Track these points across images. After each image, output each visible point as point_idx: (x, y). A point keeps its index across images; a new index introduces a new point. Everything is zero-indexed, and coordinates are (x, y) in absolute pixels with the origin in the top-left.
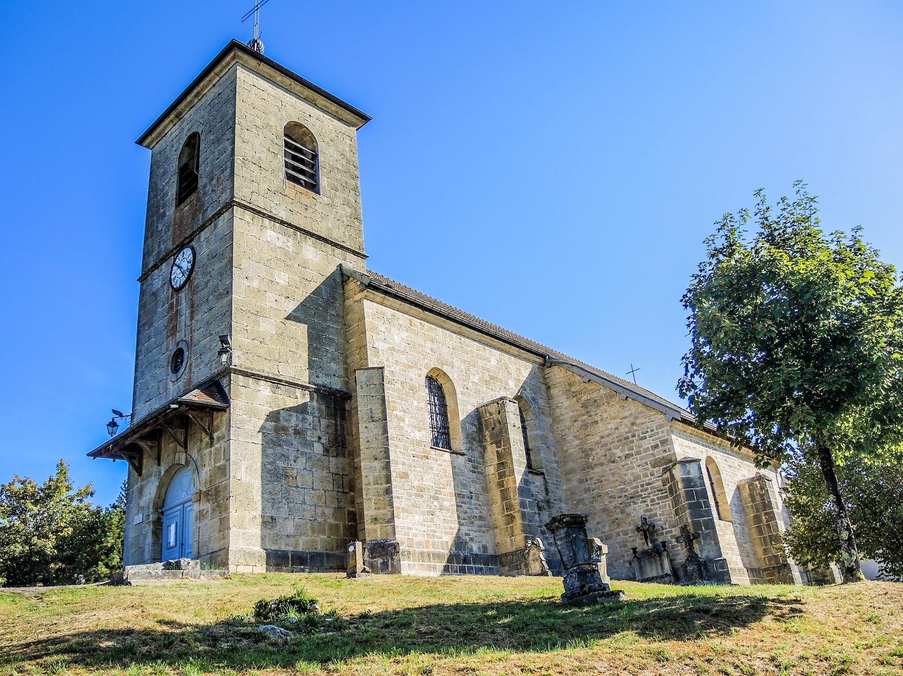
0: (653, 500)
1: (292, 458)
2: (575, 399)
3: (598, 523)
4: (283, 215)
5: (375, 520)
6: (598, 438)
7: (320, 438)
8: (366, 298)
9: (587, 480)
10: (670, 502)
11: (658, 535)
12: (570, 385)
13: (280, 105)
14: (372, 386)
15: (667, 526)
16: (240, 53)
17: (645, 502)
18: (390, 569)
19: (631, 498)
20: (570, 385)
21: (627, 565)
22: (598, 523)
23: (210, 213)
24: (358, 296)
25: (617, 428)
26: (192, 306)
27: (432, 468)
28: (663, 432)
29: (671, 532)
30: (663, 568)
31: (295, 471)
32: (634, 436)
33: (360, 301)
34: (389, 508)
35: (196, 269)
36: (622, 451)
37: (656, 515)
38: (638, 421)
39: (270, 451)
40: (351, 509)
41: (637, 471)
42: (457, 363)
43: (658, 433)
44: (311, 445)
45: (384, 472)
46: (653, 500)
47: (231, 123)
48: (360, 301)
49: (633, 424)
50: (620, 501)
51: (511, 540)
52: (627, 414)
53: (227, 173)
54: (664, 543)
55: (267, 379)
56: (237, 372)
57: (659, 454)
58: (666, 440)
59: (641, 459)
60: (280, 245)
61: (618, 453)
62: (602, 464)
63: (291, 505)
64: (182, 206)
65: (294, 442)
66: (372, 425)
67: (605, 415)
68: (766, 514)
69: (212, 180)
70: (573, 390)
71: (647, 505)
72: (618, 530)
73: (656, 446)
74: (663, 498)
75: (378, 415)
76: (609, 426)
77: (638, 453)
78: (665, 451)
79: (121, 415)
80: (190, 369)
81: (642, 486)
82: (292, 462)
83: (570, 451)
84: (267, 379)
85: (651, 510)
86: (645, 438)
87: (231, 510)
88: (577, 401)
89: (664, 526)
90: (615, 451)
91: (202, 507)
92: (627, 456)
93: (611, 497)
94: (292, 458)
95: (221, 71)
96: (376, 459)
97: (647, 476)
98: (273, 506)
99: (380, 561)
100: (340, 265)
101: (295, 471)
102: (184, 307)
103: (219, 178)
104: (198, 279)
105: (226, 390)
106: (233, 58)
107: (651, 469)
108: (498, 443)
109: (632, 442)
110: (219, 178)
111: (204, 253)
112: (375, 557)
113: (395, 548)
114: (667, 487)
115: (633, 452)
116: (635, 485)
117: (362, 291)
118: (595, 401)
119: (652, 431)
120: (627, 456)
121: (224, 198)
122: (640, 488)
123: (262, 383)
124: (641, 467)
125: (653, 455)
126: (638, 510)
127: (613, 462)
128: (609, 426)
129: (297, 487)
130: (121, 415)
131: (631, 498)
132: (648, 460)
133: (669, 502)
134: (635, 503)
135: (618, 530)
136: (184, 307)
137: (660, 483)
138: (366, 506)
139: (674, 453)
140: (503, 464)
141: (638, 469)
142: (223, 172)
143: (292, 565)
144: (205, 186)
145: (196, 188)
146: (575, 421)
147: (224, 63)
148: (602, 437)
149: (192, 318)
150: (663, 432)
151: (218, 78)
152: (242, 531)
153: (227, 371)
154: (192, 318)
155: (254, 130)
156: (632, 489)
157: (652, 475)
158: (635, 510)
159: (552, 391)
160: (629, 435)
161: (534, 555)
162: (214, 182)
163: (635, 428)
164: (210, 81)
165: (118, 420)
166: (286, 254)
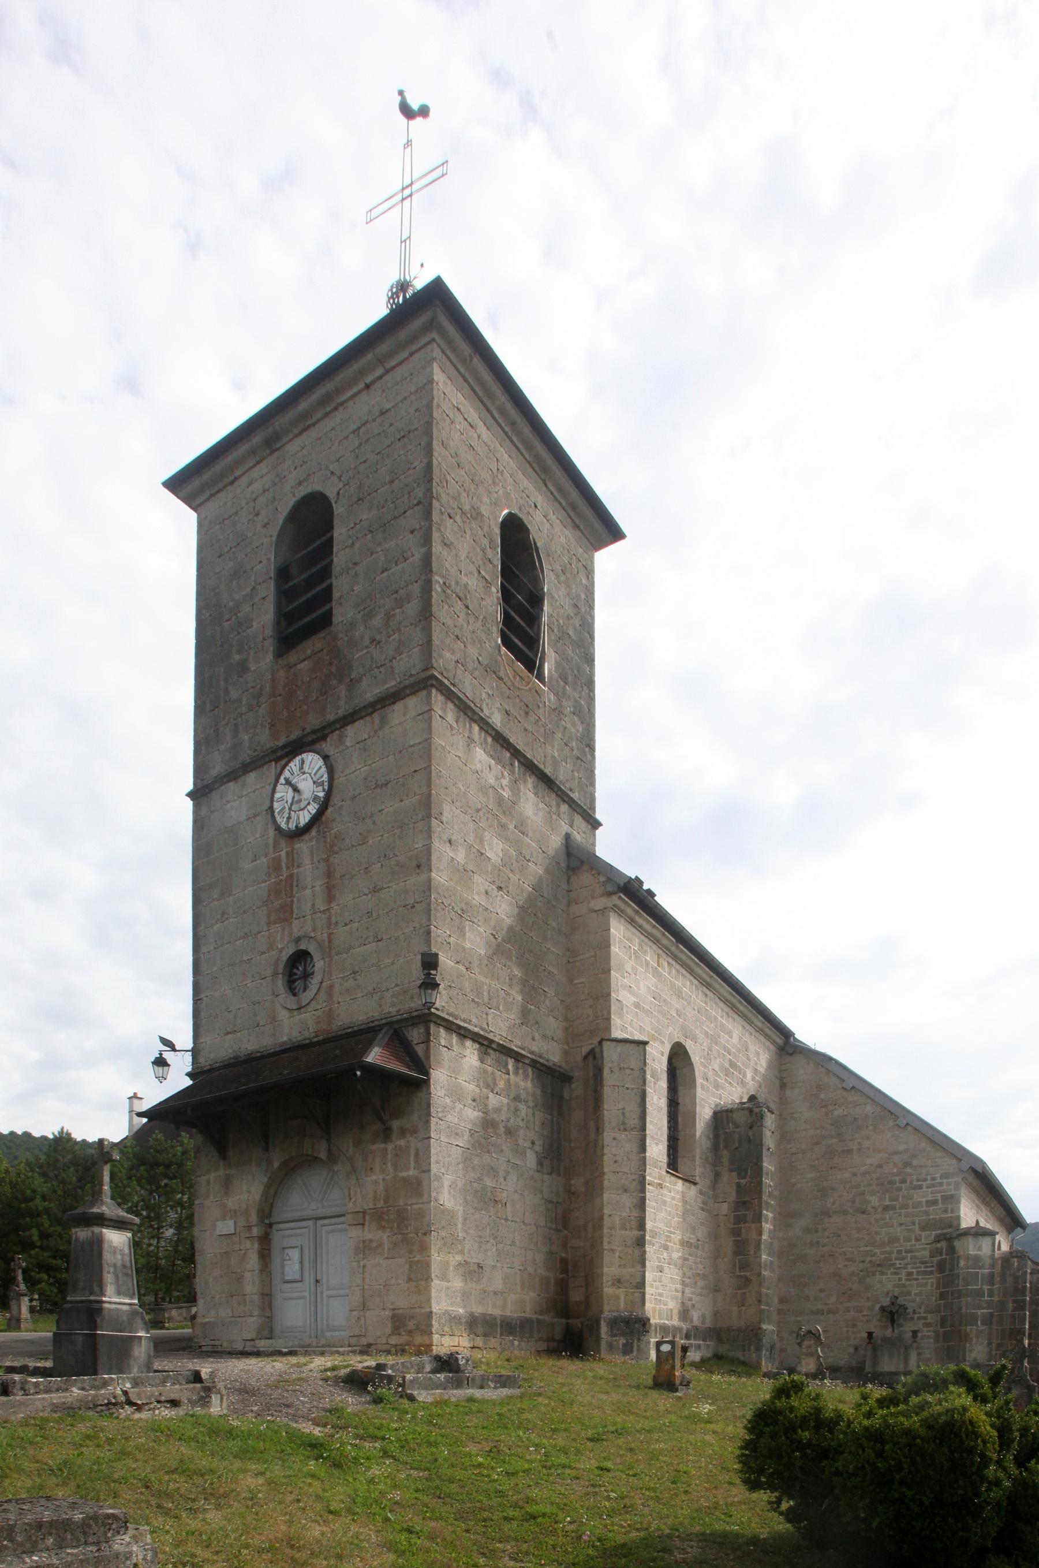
0: (910, 1274)
1: (501, 1173)
2: (823, 1110)
3: (822, 1291)
4: (497, 720)
5: (618, 1282)
6: (847, 1175)
7: (533, 1143)
8: (615, 908)
9: (817, 1231)
10: (934, 1281)
11: (905, 1319)
12: (820, 1088)
13: (495, 470)
14: (628, 1071)
15: (922, 1310)
16: (443, 320)
17: (896, 1274)
18: (635, 1353)
19: (879, 1265)
20: (820, 1088)
21: (852, 1350)
22: (822, 1291)
23: (369, 692)
24: (600, 903)
25: (880, 1166)
26: (329, 874)
27: (664, 1203)
28: (949, 1184)
29: (926, 1318)
30: (906, 1363)
31: (505, 1194)
32: (903, 1181)
33: (603, 911)
34: (639, 1267)
35: (335, 800)
36: (880, 1200)
37: (909, 1294)
38: (915, 1162)
39: (477, 1161)
40: (564, 1255)
41: (898, 1231)
42: (701, 1037)
43: (941, 1184)
44: (523, 1154)
45: (636, 1213)
46: (910, 1274)
47: (419, 493)
48: (603, 911)
49: (907, 1164)
50: (861, 1266)
51: (740, 1312)
52: (901, 1148)
53: (413, 608)
54: (915, 1333)
55: (475, 1038)
56: (451, 1027)
57: (935, 1213)
58: (952, 1197)
59: (907, 1215)
60: (492, 781)
61: (874, 1201)
62: (844, 1213)
63: (500, 1246)
64: (292, 657)
65: (505, 1148)
66: (622, 1136)
67: (866, 1144)
68: (1014, 1301)
69: (370, 615)
70: (822, 1096)
71: (900, 1279)
72: (848, 1304)
73: (934, 1202)
74: (925, 1273)
75: (633, 1121)
76: (869, 1161)
77: (904, 1206)
78: (946, 1211)
79: (173, 1049)
80: (330, 995)
81: (899, 1252)
82: (502, 1180)
83: (799, 1186)
84: (475, 1038)
85: (904, 1286)
86: (921, 1187)
87: (433, 1252)
88: (826, 1114)
89: (918, 1310)
90: (869, 1198)
91: (368, 1236)
92: (886, 1208)
93: (848, 1260)
94: (501, 1173)
95: (390, 355)
96: (626, 1191)
97: (910, 1240)
98: (480, 1247)
99: (622, 1340)
100: (568, 837)
101: (505, 1194)
102: (308, 870)
103: (388, 617)
104: (340, 821)
105: (420, 1050)
106: (427, 328)
107: (918, 1232)
108: (741, 1173)
109: (899, 1189)
110: (388, 617)
111: (355, 770)
112: (616, 1335)
113: (644, 1325)
114: (935, 1260)
115: (897, 1204)
116: (888, 1249)
117: (610, 894)
118: (856, 1120)
119: (933, 1179)
120: (886, 1208)
121: (408, 663)
122: (894, 1255)
123: (469, 1043)
124: (903, 1227)
125: (926, 1213)
126: (884, 1285)
127: (864, 1212)
128: (869, 1161)
129: (506, 1219)
130: (173, 1049)
131: (879, 1265)
132: (917, 1220)
133: (932, 1281)
134: (882, 1273)
135: (848, 1304)
136: (308, 870)
137: (927, 1253)
138: (607, 1259)
139: (959, 1217)
140: (744, 1203)
141: (899, 1229)
142: (399, 603)
143: (501, 1335)
144: (352, 626)
145: (326, 621)
146: (817, 1144)
147: (402, 335)
148: (854, 1175)
149: (330, 898)
150: (949, 1184)
151: (380, 371)
152: (445, 1284)
153: (426, 1018)
154: (330, 898)
155: (458, 518)
156: (882, 1253)
157: (917, 1239)
158: (881, 1282)
159: (788, 1092)
160: (897, 1178)
161: (809, 1347)
162: (377, 621)
163: (909, 1170)
164: (362, 373)
165: (168, 1056)
166: (500, 800)
